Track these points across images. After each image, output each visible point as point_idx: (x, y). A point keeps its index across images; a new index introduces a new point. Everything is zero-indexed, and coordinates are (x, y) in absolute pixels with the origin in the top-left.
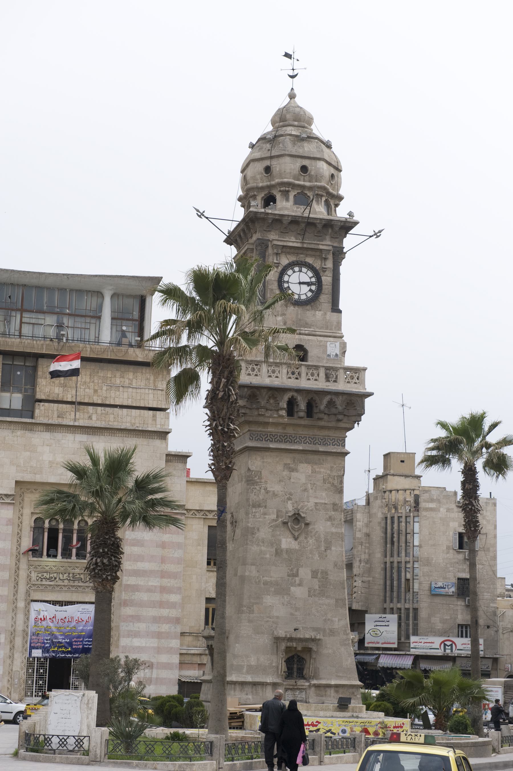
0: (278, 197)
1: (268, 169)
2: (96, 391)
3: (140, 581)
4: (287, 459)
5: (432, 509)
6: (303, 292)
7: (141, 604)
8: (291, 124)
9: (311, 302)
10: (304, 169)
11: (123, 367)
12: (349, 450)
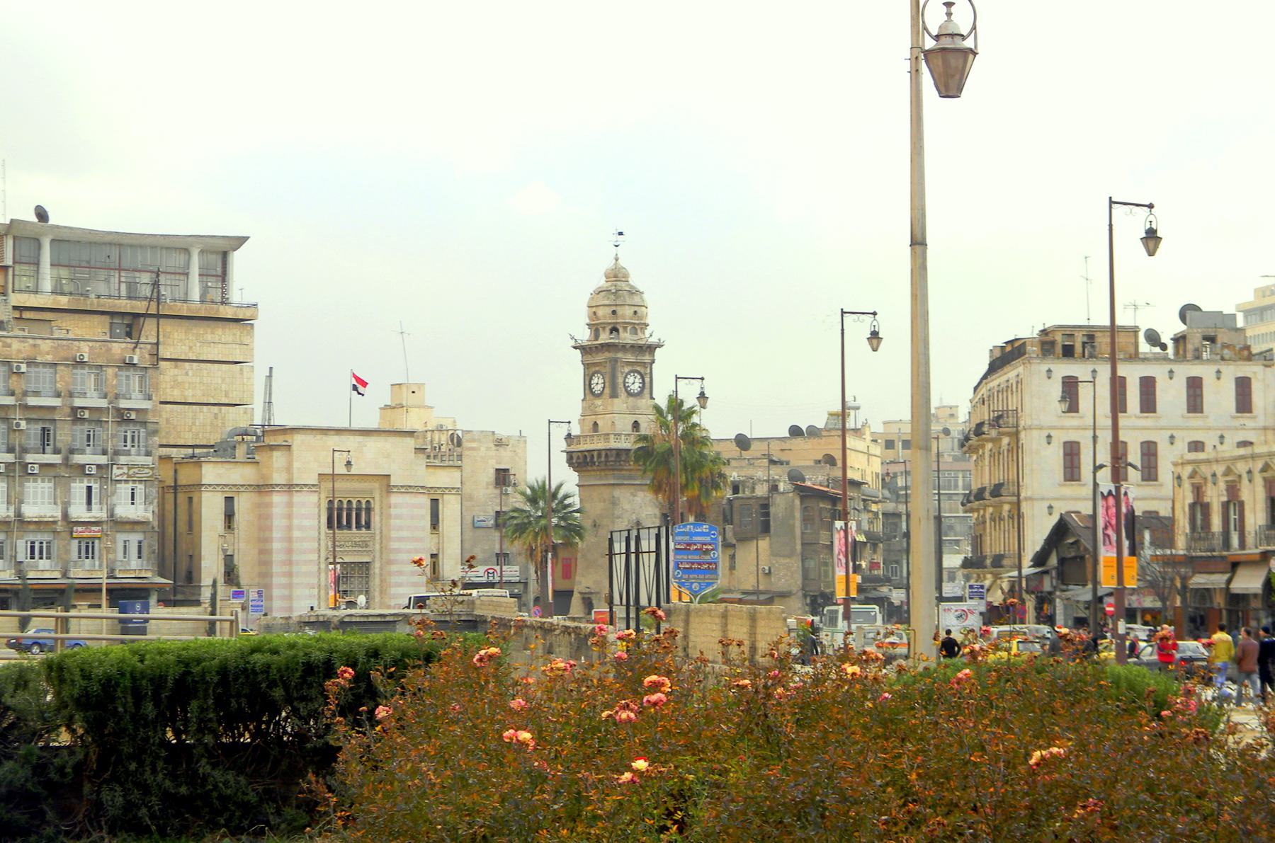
0: (621, 330)
1: (614, 312)
2: (191, 348)
3: (403, 546)
4: (632, 489)
5: (473, 449)
6: (635, 387)
8: (617, 275)
9: (639, 394)
10: (635, 312)
12: (349, 375)
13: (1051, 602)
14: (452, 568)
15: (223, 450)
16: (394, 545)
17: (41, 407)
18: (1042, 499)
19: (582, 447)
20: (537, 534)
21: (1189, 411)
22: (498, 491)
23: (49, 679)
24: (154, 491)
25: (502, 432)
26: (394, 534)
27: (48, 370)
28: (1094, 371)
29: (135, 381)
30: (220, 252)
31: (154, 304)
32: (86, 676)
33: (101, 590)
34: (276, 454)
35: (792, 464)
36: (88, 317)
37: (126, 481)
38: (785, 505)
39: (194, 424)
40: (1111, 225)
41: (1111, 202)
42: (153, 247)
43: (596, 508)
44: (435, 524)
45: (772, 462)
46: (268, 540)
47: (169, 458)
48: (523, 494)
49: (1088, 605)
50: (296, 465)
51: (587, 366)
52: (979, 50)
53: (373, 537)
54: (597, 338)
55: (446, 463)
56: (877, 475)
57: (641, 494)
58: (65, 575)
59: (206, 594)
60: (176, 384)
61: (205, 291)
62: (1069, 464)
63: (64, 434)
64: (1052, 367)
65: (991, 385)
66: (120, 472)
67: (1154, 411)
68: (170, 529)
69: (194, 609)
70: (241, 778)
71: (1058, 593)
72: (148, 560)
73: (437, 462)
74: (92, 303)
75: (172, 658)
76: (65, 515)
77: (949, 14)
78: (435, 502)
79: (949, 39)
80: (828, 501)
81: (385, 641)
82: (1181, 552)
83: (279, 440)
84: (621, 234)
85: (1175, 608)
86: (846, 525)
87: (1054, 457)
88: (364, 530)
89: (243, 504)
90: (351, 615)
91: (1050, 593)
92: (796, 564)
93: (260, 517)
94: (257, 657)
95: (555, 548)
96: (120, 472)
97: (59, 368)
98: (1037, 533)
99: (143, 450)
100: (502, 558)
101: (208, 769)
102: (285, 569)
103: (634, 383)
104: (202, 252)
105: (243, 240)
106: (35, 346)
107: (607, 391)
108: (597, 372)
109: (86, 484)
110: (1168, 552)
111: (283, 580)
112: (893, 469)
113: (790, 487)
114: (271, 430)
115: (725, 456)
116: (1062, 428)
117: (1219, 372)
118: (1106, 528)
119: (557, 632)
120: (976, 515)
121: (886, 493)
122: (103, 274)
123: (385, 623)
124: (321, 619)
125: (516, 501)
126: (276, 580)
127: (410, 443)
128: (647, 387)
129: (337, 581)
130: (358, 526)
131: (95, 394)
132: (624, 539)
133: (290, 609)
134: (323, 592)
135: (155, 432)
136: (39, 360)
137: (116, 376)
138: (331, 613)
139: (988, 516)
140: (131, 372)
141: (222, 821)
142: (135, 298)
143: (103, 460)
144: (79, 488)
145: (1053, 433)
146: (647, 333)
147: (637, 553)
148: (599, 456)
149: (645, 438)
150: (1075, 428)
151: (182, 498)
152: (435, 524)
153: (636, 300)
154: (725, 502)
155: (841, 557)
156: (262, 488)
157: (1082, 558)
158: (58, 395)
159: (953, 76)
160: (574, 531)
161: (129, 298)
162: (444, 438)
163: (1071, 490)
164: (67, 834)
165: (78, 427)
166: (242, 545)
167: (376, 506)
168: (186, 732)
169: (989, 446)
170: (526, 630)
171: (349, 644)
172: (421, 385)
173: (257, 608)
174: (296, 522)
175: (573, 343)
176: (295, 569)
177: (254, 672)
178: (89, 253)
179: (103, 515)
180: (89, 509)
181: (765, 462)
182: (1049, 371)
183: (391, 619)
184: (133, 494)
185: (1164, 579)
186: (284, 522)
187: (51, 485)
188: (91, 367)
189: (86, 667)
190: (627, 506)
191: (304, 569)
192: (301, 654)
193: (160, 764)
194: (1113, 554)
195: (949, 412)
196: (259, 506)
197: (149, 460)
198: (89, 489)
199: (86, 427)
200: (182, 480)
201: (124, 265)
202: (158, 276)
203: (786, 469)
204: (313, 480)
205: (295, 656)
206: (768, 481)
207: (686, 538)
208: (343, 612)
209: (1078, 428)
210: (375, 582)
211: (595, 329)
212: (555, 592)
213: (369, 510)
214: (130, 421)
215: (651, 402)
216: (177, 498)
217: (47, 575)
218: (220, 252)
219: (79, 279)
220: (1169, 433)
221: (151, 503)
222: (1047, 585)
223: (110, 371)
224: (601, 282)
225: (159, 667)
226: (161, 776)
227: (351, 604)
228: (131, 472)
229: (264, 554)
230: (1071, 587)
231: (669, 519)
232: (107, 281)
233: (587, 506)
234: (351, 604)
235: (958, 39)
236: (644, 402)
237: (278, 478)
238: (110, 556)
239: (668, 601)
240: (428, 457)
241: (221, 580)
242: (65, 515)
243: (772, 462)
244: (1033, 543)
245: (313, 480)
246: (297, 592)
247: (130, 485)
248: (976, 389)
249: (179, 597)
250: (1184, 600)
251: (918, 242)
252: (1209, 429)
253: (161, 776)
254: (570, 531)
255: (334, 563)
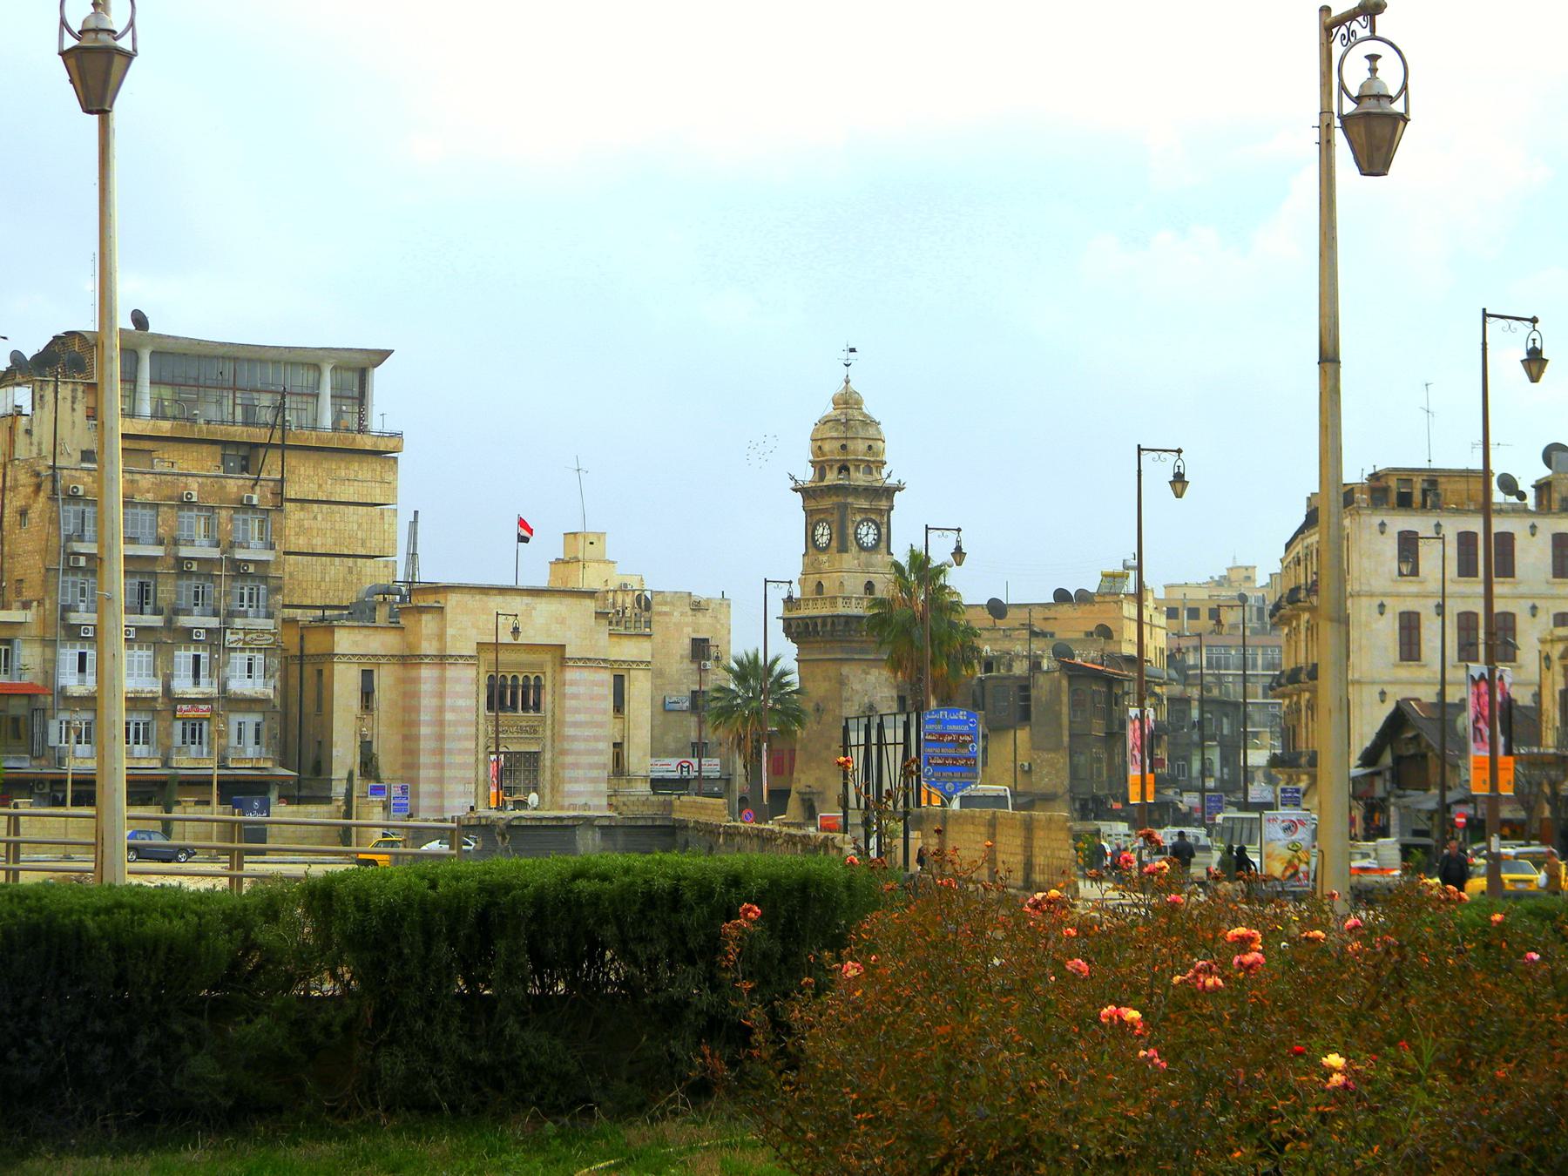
1: (844, 447)
2: (320, 486)
5: (666, 614)
6: (869, 540)
7: (579, 753)
8: (847, 401)
9: (874, 548)
10: (870, 447)
11: (348, 457)
13: (1384, 810)
14: (640, 761)
15: (361, 612)
16: (569, 731)
17: (139, 557)
18: (1373, 683)
19: (803, 613)
20: (746, 720)
21: (1555, 576)
22: (695, 666)
23: (309, 909)
24: (276, 662)
25: (701, 593)
26: (569, 718)
27: (148, 512)
28: (1438, 526)
29: (254, 526)
30: (357, 370)
31: (278, 433)
32: (364, 907)
33: (211, 783)
34: (425, 618)
35: (1057, 636)
36: (195, 447)
37: (242, 650)
38: (1049, 686)
39: (323, 579)
40: (1484, 344)
41: (1485, 315)
42: (276, 362)
43: (819, 689)
44: (619, 707)
45: (1033, 634)
46: (414, 724)
47: (294, 621)
48: (729, 670)
49: (1431, 814)
50: (450, 631)
51: (809, 513)
52: (1412, 115)
53: (543, 720)
54: (822, 478)
55: (633, 631)
56: (1162, 651)
57: (875, 672)
58: (166, 763)
59: (339, 789)
60: (302, 530)
61: (338, 416)
62: (1406, 640)
63: (166, 591)
64: (1387, 520)
65: (1309, 541)
66: (235, 637)
67: (1512, 575)
68: (295, 710)
69: (323, 808)
70: (557, 1042)
71: (1392, 800)
72: (267, 747)
73: (621, 630)
74: (201, 430)
75: (474, 885)
76: (167, 689)
77: (1373, 70)
78: (619, 681)
79: (1373, 102)
80: (1102, 684)
81: (747, 865)
82: (1551, 751)
83: (429, 601)
84: (853, 350)
85: (1542, 820)
86: (1142, 712)
87: (1387, 631)
88: (532, 713)
89: (385, 679)
90: (520, 818)
91: (1383, 800)
92: (1062, 760)
93: (405, 695)
94: (581, 884)
95: (770, 737)
96: (235, 637)
97: (161, 509)
98: (1368, 723)
99: (263, 611)
100: (699, 749)
101: (516, 1028)
102: (435, 759)
103: (868, 535)
104: (335, 368)
105: (385, 354)
106: (132, 481)
107: (834, 544)
108: (822, 521)
109: (192, 652)
110: (1535, 750)
111: (432, 773)
112: (1183, 643)
113: (1055, 664)
114: (415, 588)
115: (976, 625)
116: (1398, 595)
117: (1533, 527)
118: (1476, 720)
119: (780, 841)
120: (1287, 702)
121: (1173, 673)
122: (214, 394)
123: (561, 831)
124: (483, 822)
125: (718, 677)
126: (423, 773)
127: (590, 605)
128: (884, 539)
129: (501, 774)
130: (525, 708)
131: (205, 542)
132: (862, 727)
133: (441, 809)
134: (481, 789)
135: (278, 589)
136: (138, 499)
137: (231, 519)
138: (494, 814)
139: (1303, 703)
140: (249, 516)
141: (533, 1098)
142: (254, 424)
143: (214, 622)
144: (184, 657)
145: (1386, 601)
146: (884, 473)
147: (880, 744)
148: (824, 625)
149: (880, 603)
150: (1417, 596)
151: (309, 670)
152: (619, 707)
153: (872, 432)
154: (975, 682)
155: (1136, 752)
156: (408, 660)
157: (1424, 756)
158: (160, 542)
159: (1378, 149)
160: (791, 715)
161: (245, 424)
162: (629, 600)
163: (1407, 672)
164: (331, 1110)
165: (184, 583)
166: (383, 730)
167: (548, 683)
168: (483, 978)
169: (1305, 616)
170: (738, 839)
171: (703, 869)
172: (601, 535)
173: (400, 807)
174: (448, 702)
175: (792, 484)
176: (447, 759)
177: (579, 905)
178: (193, 369)
179: (213, 691)
180: (197, 683)
181: (1025, 633)
182: (1383, 524)
183: (570, 823)
184: (250, 665)
185: (1529, 783)
186: (435, 702)
187: (151, 653)
188: (200, 508)
189: (362, 896)
190: (857, 686)
191: (458, 759)
192: (639, 881)
193: (455, 1023)
194: (1485, 753)
195: (1245, 574)
196: (404, 681)
197: (269, 624)
198: (197, 658)
199: (194, 582)
200: (311, 648)
201: (239, 384)
202: (283, 397)
203: (1050, 642)
204: (470, 650)
205: (632, 884)
206: (1028, 657)
207: (939, 727)
208: (510, 813)
209: (1417, 596)
210: (546, 776)
211: (820, 467)
212: (770, 792)
213: (538, 687)
214: (246, 575)
215: (888, 558)
216: (303, 670)
217: (144, 764)
218: (357, 370)
219: (185, 401)
220: (1530, 602)
221: (272, 676)
222: (1379, 789)
223: (224, 513)
224: (828, 409)
225: (456, 895)
226: (454, 1038)
227: (521, 804)
228: (248, 638)
229: (409, 740)
230: (1409, 792)
231: (910, 703)
232: (219, 403)
233: (809, 686)
234: (521, 804)
235: (1384, 102)
236: (880, 558)
237: (428, 647)
238: (222, 741)
239: (919, 805)
240: (610, 623)
241: (357, 772)
242: (167, 689)
243: (1033, 634)
244: (1361, 736)
245: (470, 650)
246: (450, 788)
247: (247, 654)
248: (1288, 546)
249: (304, 793)
250: (1554, 810)
251: (1329, 358)
252: (1521, 597)
253: (454, 1038)
254: (787, 715)
255: (497, 752)
